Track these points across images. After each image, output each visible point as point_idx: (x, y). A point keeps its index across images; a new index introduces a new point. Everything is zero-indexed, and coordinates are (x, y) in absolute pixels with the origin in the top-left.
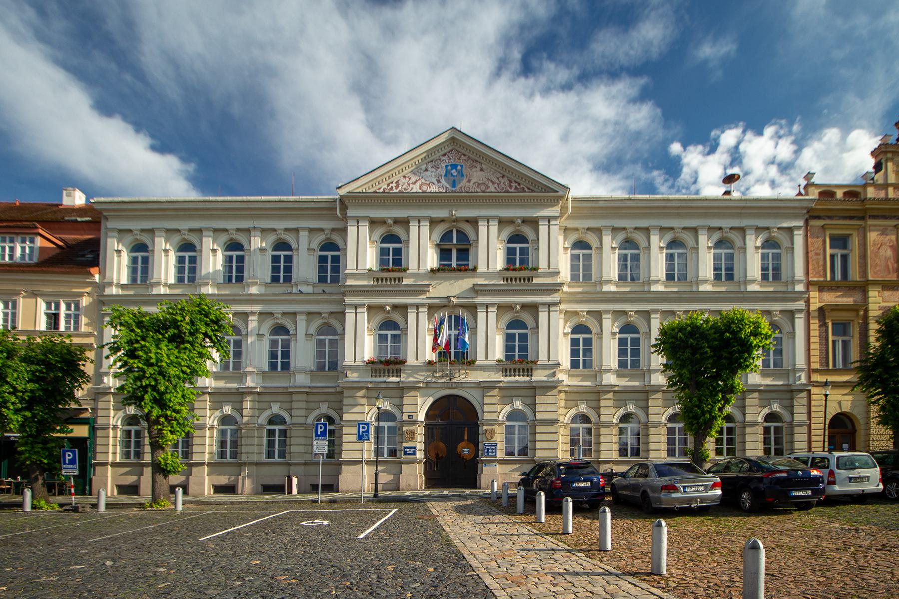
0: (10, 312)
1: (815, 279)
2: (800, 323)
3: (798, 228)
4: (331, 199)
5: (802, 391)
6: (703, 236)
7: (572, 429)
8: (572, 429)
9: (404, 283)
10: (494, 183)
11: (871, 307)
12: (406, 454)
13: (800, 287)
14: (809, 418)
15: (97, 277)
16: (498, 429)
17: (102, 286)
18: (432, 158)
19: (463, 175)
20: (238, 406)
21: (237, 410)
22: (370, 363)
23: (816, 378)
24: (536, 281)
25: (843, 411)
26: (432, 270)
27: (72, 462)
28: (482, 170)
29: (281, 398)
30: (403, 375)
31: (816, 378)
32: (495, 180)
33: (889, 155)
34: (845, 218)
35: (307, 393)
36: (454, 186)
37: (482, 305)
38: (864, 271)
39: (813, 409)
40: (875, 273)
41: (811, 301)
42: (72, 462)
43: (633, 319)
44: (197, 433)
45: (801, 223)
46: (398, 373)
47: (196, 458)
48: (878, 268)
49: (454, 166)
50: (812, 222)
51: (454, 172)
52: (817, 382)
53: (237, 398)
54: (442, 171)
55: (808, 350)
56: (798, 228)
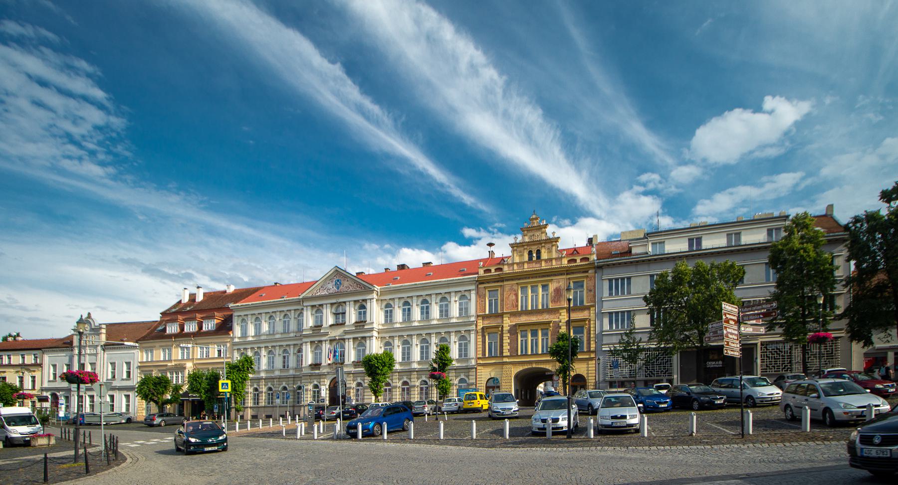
0: (202, 351)
1: (481, 314)
2: (473, 336)
3: (473, 290)
4: (296, 299)
5: (473, 368)
6: (726, 242)
7: (459, 386)
8: (459, 386)
9: (321, 332)
10: (351, 286)
11: (504, 325)
12: (321, 402)
13: (473, 319)
14: (476, 381)
15: (232, 336)
16: (352, 391)
17: (233, 338)
18: (329, 279)
19: (341, 284)
20: (467, 374)
21: (467, 376)
22: (310, 365)
23: (481, 362)
24: (365, 327)
25: (577, 373)
26: (331, 326)
27: (216, 408)
28: (347, 281)
29: (360, 375)
30: (321, 369)
31: (481, 362)
32: (352, 285)
33: (543, 245)
34: (495, 282)
35: (310, 376)
36: (338, 289)
37: (347, 339)
38: (502, 308)
39: (478, 377)
40: (507, 308)
41: (479, 324)
42: (216, 408)
43: (443, 335)
44: (246, 395)
45: (473, 287)
46: (319, 369)
47: (246, 405)
48: (508, 306)
49: (338, 281)
50: (480, 286)
51: (338, 283)
52: (480, 364)
53: (257, 381)
54: (334, 283)
55: (476, 349)
56: (473, 290)
